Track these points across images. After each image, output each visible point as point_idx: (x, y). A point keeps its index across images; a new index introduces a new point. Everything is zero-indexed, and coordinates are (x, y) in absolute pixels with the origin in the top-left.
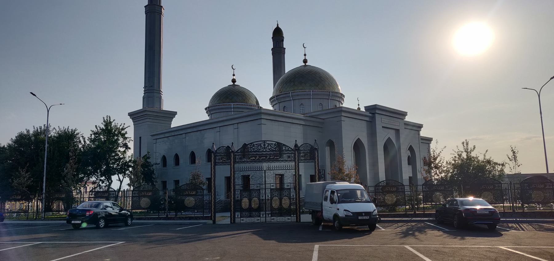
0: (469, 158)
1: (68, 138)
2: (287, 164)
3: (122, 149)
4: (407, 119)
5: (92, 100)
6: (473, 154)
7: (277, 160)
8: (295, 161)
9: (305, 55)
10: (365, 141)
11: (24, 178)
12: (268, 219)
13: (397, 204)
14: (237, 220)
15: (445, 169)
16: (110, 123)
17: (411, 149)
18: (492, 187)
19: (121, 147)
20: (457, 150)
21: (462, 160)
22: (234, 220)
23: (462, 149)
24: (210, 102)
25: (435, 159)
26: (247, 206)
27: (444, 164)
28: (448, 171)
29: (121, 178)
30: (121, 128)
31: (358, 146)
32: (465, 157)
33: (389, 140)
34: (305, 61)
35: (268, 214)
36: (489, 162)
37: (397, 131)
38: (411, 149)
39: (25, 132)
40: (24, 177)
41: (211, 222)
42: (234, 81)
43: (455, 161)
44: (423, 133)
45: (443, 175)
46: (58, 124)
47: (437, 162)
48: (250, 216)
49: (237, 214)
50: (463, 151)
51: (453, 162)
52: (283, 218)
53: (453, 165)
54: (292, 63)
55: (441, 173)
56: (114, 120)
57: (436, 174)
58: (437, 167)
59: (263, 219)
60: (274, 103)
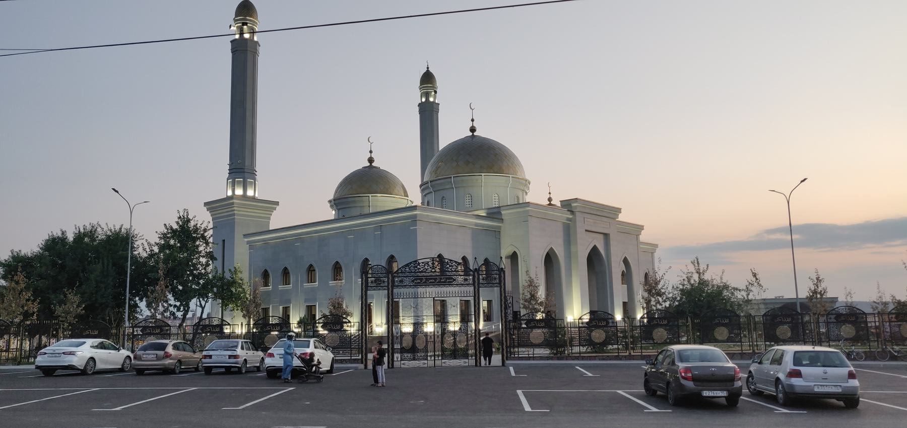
0: (703, 283)
1: (120, 242)
2: (463, 289)
3: (203, 260)
4: (621, 218)
5: (153, 184)
6: (707, 277)
7: (450, 284)
8: (474, 284)
9: (473, 120)
10: (560, 252)
11: (72, 303)
12: (438, 363)
13: (606, 343)
14: (396, 364)
15: (671, 295)
16: (189, 221)
17: (626, 261)
18: (604, 323)
19: (203, 257)
20: (686, 271)
21: (692, 285)
22: (393, 365)
23: (692, 269)
24: (336, 192)
25: (657, 283)
26: (410, 344)
27: (670, 288)
28: (674, 299)
29: (203, 303)
30: (203, 226)
31: (550, 259)
32: (697, 280)
33: (595, 250)
34: (473, 130)
35: (438, 356)
36: (726, 287)
37: (606, 236)
38: (626, 261)
39: (60, 234)
40: (72, 304)
41: (362, 366)
42: (371, 160)
43: (683, 285)
44: (644, 237)
45: (667, 304)
46: (107, 218)
47: (660, 286)
48: (414, 359)
49: (396, 355)
50: (694, 271)
51: (681, 287)
52: (458, 361)
53: (682, 290)
54: (450, 132)
55: (665, 301)
56: (195, 217)
57: (659, 302)
58: (659, 294)
59: (431, 363)
60: (426, 192)
